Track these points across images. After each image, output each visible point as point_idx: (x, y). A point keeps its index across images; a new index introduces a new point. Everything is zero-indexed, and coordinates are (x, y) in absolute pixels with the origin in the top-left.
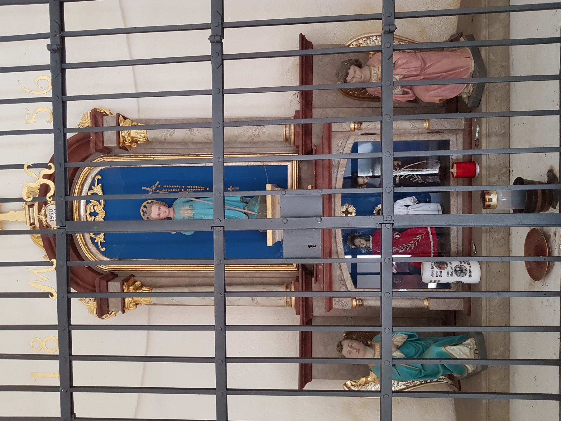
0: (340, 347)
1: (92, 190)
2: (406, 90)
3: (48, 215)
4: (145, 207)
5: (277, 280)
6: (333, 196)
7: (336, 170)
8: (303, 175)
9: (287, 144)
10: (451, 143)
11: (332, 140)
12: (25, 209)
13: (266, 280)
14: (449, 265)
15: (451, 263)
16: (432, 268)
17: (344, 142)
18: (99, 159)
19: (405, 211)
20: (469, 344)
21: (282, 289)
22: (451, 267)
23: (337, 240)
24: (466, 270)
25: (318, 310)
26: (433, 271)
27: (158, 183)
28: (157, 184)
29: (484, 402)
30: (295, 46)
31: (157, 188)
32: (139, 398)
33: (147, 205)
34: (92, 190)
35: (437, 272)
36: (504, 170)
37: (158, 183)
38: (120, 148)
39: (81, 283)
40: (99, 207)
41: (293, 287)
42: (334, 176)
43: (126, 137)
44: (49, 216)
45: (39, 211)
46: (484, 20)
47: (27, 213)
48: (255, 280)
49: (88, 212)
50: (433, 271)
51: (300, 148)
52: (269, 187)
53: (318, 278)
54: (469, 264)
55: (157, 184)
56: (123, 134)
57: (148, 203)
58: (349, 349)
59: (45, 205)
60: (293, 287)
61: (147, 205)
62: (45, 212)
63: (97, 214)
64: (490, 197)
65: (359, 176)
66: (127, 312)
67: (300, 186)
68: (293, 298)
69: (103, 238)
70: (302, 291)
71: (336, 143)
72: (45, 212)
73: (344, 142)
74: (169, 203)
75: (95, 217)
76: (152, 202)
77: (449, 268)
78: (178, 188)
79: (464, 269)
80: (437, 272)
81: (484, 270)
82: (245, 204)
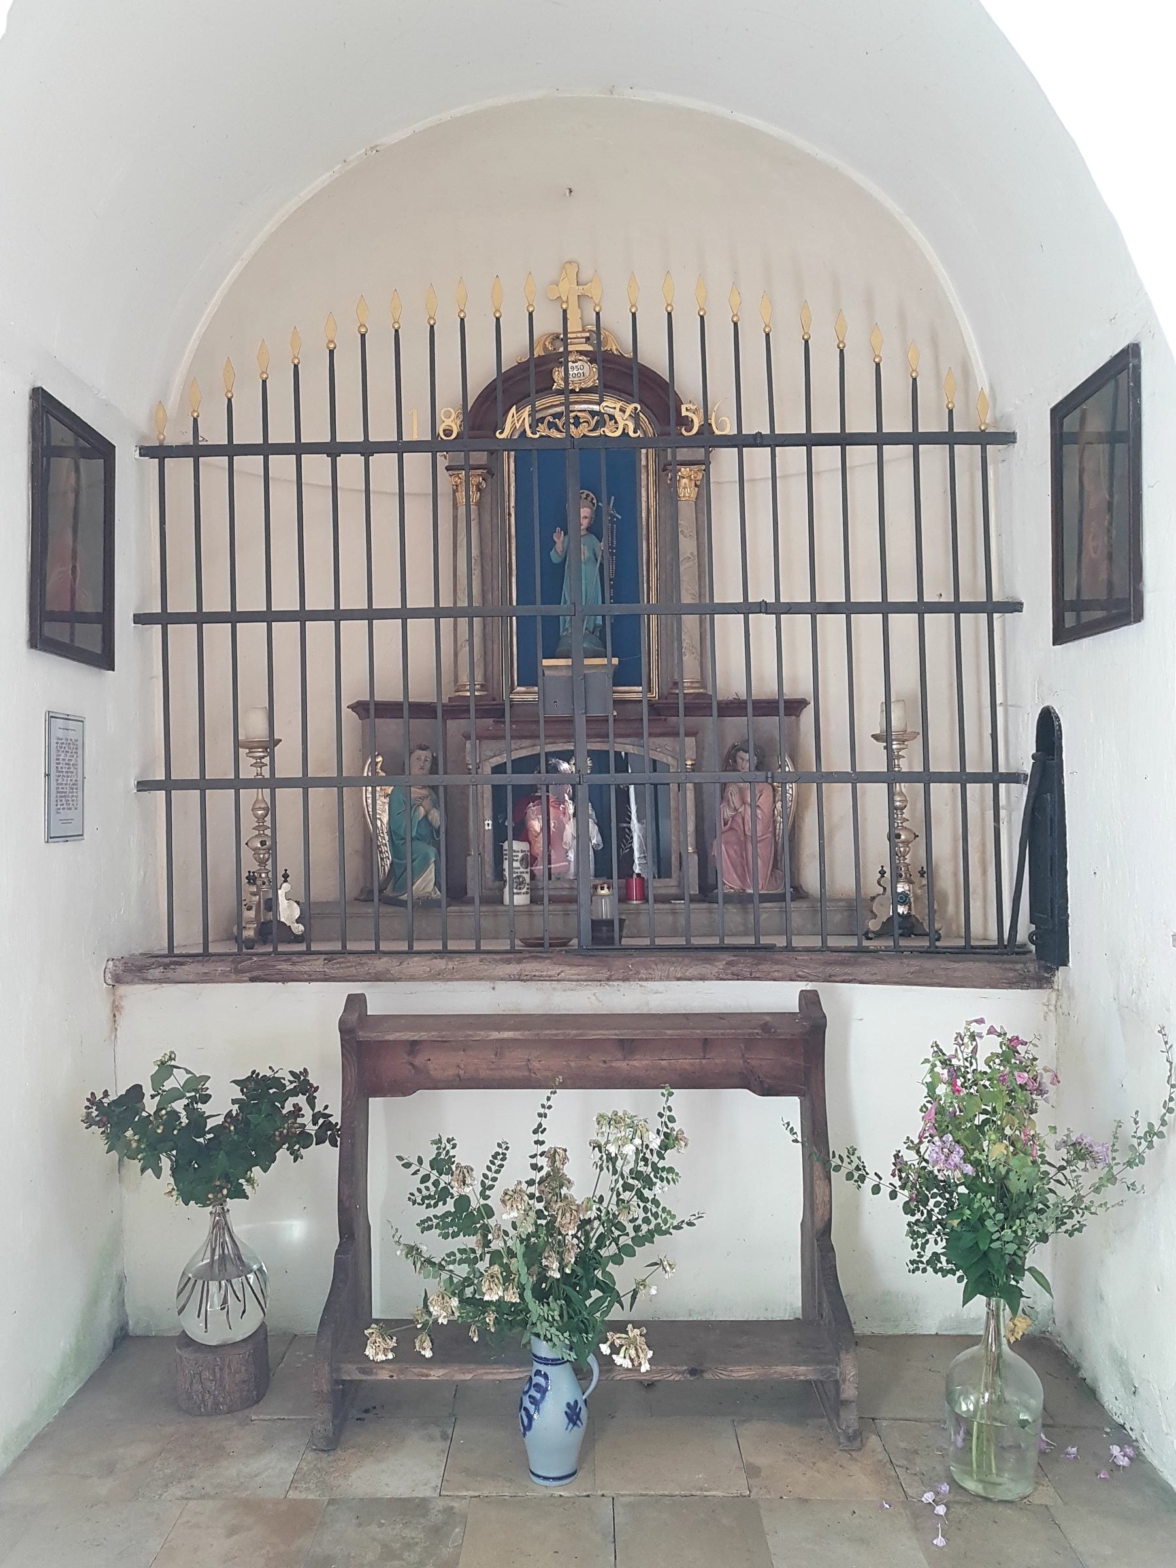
0: (423, 748)
1: (610, 420)
2: (729, 823)
3: (576, 364)
4: (588, 495)
5: (489, 673)
6: (606, 739)
7: (636, 743)
8: (629, 706)
9: (670, 685)
10: (668, 880)
11: (672, 739)
12: (584, 331)
13: (489, 658)
14: (525, 870)
15: (527, 872)
16: (522, 851)
17: (671, 754)
18: (652, 431)
19: (647, 453)
20: (435, 893)
21: (479, 679)
22: (523, 873)
23: (551, 745)
24: (520, 889)
25: (455, 726)
26: (518, 852)
27: (620, 517)
28: (617, 515)
29: (370, 910)
30: (789, 693)
31: (613, 516)
32: (328, 487)
33: (589, 498)
34: (610, 420)
35: (517, 856)
36: (635, 931)
37: (620, 517)
38: (665, 466)
39: (486, 405)
40: (586, 430)
41: (482, 693)
42: (628, 740)
43: (680, 474)
44: (574, 365)
45: (581, 353)
46: (805, 906)
47: (579, 335)
48: (489, 643)
49: (579, 414)
50: (518, 852)
51: (665, 701)
52: (615, 661)
53: (499, 724)
54: (527, 893)
55: (617, 515)
56: (683, 469)
57: (593, 499)
58: (423, 758)
59: (589, 361)
60: (482, 693)
61: (589, 498)
62: (580, 360)
63: (576, 427)
64: (606, 888)
65: (571, 352)
66: (447, 473)
67: (617, 702)
68: (468, 694)
69: (544, 434)
70: (476, 705)
71: (667, 741)
72: (580, 360)
73: (671, 754)
74: (594, 529)
75: (573, 423)
76: (593, 504)
77: (522, 870)
78: (612, 543)
79: (522, 886)
80: (517, 856)
81: (521, 909)
82: (591, 630)
